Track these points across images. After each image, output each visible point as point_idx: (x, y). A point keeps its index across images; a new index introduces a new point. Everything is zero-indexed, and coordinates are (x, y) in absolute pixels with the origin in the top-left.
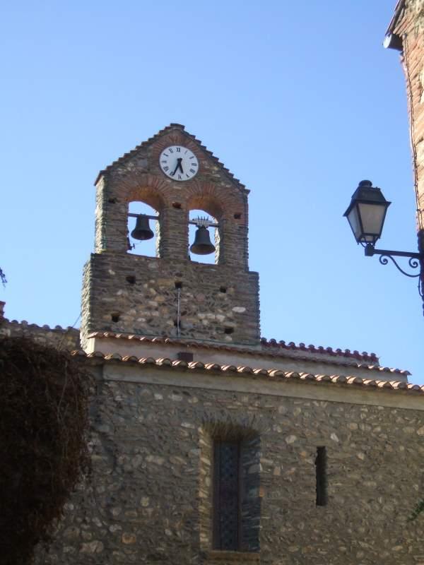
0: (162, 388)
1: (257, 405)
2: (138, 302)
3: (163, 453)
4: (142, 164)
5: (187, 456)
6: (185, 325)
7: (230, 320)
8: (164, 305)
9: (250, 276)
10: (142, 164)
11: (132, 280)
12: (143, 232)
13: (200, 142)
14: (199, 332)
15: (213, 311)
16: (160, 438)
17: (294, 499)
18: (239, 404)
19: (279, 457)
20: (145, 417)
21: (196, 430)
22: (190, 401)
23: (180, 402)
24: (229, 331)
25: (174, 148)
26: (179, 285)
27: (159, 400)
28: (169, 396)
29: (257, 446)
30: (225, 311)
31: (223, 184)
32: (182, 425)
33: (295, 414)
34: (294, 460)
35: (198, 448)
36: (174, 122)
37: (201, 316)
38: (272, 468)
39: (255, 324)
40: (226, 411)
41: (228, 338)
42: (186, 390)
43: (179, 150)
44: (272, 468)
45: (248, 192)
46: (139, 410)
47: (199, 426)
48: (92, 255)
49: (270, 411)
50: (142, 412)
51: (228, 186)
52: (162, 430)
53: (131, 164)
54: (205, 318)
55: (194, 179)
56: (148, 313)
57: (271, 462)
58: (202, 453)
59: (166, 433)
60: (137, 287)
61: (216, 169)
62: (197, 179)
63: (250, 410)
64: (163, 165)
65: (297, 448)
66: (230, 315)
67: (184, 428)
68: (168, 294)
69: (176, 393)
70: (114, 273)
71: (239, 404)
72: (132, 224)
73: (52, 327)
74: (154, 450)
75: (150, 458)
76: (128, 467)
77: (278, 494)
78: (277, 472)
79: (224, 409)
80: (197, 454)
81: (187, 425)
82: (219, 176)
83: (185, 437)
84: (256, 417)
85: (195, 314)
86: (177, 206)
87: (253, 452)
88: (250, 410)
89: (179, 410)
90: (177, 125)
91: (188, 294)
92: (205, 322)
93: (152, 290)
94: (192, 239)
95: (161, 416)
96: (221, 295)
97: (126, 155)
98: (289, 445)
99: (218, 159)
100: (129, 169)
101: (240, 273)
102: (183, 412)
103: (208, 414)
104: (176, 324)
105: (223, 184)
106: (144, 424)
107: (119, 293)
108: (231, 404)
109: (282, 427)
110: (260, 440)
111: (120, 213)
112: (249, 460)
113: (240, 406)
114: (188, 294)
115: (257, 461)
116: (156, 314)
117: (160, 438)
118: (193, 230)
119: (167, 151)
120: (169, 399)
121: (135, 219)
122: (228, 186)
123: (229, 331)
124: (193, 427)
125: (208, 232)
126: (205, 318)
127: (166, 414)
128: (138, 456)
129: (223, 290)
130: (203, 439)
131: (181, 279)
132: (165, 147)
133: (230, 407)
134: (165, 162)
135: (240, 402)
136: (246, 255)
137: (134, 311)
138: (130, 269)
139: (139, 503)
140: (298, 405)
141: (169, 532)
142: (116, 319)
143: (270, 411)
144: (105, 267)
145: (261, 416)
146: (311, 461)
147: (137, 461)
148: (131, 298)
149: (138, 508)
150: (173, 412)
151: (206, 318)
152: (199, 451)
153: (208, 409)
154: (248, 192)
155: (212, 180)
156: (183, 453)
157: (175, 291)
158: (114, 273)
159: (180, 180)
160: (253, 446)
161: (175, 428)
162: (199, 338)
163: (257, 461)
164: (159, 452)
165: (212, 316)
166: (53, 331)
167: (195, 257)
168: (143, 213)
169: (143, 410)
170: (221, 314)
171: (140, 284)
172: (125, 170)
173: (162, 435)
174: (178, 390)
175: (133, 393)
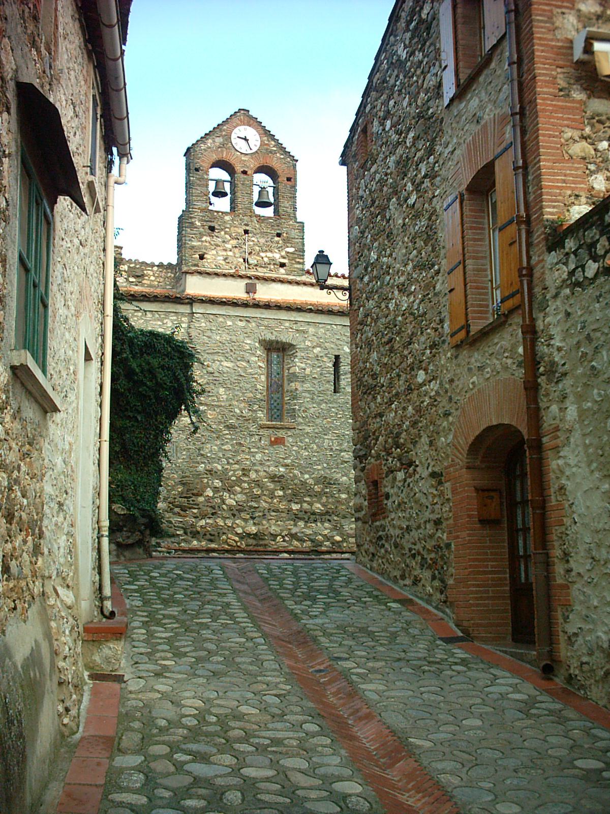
2: (217, 246)
4: (219, 140)
6: (251, 261)
7: (284, 258)
8: (236, 247)
9: (297, 225)
10: (219, 140)
11: (212, 229)
12: (219, 194)
14: (261, 267)
17: (319, 389)
24: (282, 265)
26: (246, 232)
31: (278, 155)
37: (263, 254)
38: (304, 369)
39: (301, 261)
41: (282, 270)
44: (304, 369)
48: (183, 211)
51: (282, 157)
54: (266, 256)
56: (225, 253)
57: (303, 365)
60: (216, 234)
61: (273, 143)
66: (283, 253)
70: (199, 224)
72: (212, 187)
73: (157, 264)
75: (225, 364)
76: (210, 369)
77: (307, 386)
78: (308, 371)
81: (249, 342)
82: (275, 149)
86: (245, 172)
91: (253, 239)
92: (266, 260)
93: (227, 236)
94: (255, 198)
96: (277, 239)
100: (209, 145)
101: (291, 223)
104: (244, 261)
105: (278, 155)
107: (204, 239)
112: (289, 364)
114: (253, 239)
116: (230, 254)
118: (256, 190)
122: (282, 157)
123: (282, 265)
126: (266, 256)
129: (279, 235)
131: (247, 228)
132: (235, 127)
136: (295, 209)
137: (214, 252)
138: (211, 222)
139: (218, 392)
141: (237, 411)
142: (202, 257)
144: (193, 220)
146: (331, 365)
147: (216, 366)
148: (212, 243)
149: (218, 395)
151: (266, 256)
155: (271, 152)
157: (244, 237)
158: (199, 224)
162: (261, 272)
165: (269, 254)
166: (157, 266)
167: (259, 211)
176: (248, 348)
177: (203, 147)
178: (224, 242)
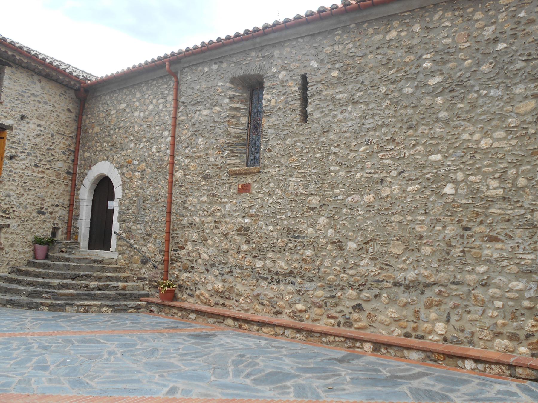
18: (250, 58)
71: (250, 58)
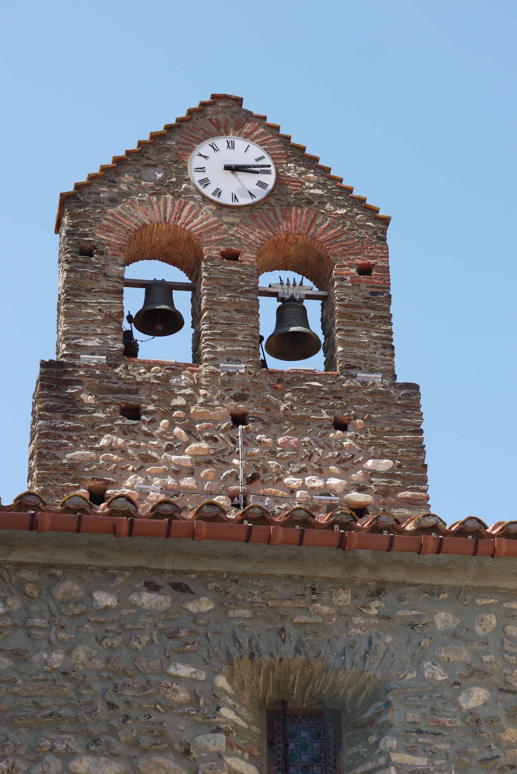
0: (114, 577)
1: (375, 612)
3: (118, 748)
5: (187, 752)
7: (361, 489)
8: (209, 463)
13: (277, 128)
15: (320, 472)
16: (111, 706)
18: (326, 609)
19: (442, 746)
20: (69, 653)
21: (210, 681)
22: (191, 607)
23: (167, 611)
25: (221, 142)
27: (107, 608)
28: (134, 598)
29: (381, 720)
30: (346, 469)
32: (172, 670)
33: (479, 630)
34: (487, 754)
35: (218, 730)
36: (219, 91)
40: (292, 632)
42: (177, 579)
43: (231, 146)
45: (386, 221)
46: (53, 637)
47: (219, 672)
48: (44, 364)
49: (413, 626)
50: (62, 641)
52: (116, 686)
53: (127, 178)
55: (265, 200)
58: (230, 744)
59: (128, 693)
62: (272, 201)
63: (357, 626)
64: (196, 177)
65: (491, 721)
66: (357, 476)
67: (177, 678)
68: (216, 440)
69: (153, 587)
74: (96, 741)
79: (287, 625)
80: (212, 748)
83: (181, 705)
84: (375, 641)
85: (280, 480)
87: (372, 739)
88: (357, 626)
89: (161, 631)
90: (479, 521)
95: (111, 648)
97: (118, 161)
98: (471, 712)
99: (329, 170)
100: (124, 187)
102: (172, 636)
103: (244, 640)
106: (65, 673)
107: (104, 442)
108: (306, 610)
109: (447, 665)
110: (388, 704)
111: (105, 275)
113: (329, 616)
115: (382, 761)
116: (188, 482)
117: (111, 706)
119: (205, 148)
120: (134, 606)
121: (141, 292)
124: (202, 676)
125: (304, 310)
127: (126, 644)
128: (49, 758)
130: (233, 708)
132: (200, 141)
133: (303, 619)
134: (202, 169)
135: (331, 604)
140: (487, 608)
143: (413, 626)
145: (389, 639)
150: (145, 639)
151: (303, 487)
152: (221, 738)
153: (243, 626)
154: (386, 221)
155: (309, 202)
156: (177, 746)
157: (231, 433)
159: (236, 203)
160: (371, 722)
161: (154, 679)
163: (382, 761)
164: (108, 744)
168: (159, 278)
169: (62, 635)
170: (335, 476)
171: (153, 421)
172: (115, 190)
173: (116, 700)
174: (158, 580)
175: (36, 593)
176: (183, 695)
177: (105, 192)
178: (169, 449)
